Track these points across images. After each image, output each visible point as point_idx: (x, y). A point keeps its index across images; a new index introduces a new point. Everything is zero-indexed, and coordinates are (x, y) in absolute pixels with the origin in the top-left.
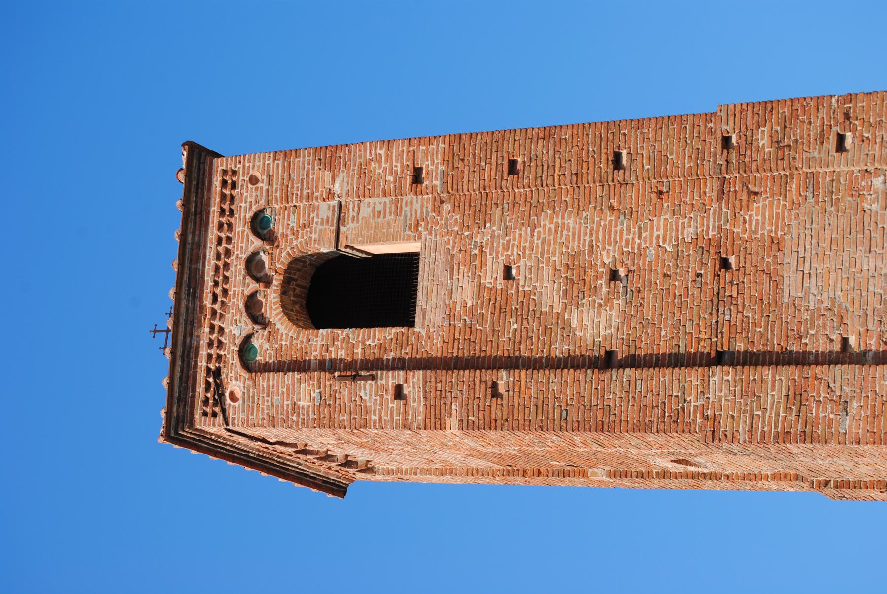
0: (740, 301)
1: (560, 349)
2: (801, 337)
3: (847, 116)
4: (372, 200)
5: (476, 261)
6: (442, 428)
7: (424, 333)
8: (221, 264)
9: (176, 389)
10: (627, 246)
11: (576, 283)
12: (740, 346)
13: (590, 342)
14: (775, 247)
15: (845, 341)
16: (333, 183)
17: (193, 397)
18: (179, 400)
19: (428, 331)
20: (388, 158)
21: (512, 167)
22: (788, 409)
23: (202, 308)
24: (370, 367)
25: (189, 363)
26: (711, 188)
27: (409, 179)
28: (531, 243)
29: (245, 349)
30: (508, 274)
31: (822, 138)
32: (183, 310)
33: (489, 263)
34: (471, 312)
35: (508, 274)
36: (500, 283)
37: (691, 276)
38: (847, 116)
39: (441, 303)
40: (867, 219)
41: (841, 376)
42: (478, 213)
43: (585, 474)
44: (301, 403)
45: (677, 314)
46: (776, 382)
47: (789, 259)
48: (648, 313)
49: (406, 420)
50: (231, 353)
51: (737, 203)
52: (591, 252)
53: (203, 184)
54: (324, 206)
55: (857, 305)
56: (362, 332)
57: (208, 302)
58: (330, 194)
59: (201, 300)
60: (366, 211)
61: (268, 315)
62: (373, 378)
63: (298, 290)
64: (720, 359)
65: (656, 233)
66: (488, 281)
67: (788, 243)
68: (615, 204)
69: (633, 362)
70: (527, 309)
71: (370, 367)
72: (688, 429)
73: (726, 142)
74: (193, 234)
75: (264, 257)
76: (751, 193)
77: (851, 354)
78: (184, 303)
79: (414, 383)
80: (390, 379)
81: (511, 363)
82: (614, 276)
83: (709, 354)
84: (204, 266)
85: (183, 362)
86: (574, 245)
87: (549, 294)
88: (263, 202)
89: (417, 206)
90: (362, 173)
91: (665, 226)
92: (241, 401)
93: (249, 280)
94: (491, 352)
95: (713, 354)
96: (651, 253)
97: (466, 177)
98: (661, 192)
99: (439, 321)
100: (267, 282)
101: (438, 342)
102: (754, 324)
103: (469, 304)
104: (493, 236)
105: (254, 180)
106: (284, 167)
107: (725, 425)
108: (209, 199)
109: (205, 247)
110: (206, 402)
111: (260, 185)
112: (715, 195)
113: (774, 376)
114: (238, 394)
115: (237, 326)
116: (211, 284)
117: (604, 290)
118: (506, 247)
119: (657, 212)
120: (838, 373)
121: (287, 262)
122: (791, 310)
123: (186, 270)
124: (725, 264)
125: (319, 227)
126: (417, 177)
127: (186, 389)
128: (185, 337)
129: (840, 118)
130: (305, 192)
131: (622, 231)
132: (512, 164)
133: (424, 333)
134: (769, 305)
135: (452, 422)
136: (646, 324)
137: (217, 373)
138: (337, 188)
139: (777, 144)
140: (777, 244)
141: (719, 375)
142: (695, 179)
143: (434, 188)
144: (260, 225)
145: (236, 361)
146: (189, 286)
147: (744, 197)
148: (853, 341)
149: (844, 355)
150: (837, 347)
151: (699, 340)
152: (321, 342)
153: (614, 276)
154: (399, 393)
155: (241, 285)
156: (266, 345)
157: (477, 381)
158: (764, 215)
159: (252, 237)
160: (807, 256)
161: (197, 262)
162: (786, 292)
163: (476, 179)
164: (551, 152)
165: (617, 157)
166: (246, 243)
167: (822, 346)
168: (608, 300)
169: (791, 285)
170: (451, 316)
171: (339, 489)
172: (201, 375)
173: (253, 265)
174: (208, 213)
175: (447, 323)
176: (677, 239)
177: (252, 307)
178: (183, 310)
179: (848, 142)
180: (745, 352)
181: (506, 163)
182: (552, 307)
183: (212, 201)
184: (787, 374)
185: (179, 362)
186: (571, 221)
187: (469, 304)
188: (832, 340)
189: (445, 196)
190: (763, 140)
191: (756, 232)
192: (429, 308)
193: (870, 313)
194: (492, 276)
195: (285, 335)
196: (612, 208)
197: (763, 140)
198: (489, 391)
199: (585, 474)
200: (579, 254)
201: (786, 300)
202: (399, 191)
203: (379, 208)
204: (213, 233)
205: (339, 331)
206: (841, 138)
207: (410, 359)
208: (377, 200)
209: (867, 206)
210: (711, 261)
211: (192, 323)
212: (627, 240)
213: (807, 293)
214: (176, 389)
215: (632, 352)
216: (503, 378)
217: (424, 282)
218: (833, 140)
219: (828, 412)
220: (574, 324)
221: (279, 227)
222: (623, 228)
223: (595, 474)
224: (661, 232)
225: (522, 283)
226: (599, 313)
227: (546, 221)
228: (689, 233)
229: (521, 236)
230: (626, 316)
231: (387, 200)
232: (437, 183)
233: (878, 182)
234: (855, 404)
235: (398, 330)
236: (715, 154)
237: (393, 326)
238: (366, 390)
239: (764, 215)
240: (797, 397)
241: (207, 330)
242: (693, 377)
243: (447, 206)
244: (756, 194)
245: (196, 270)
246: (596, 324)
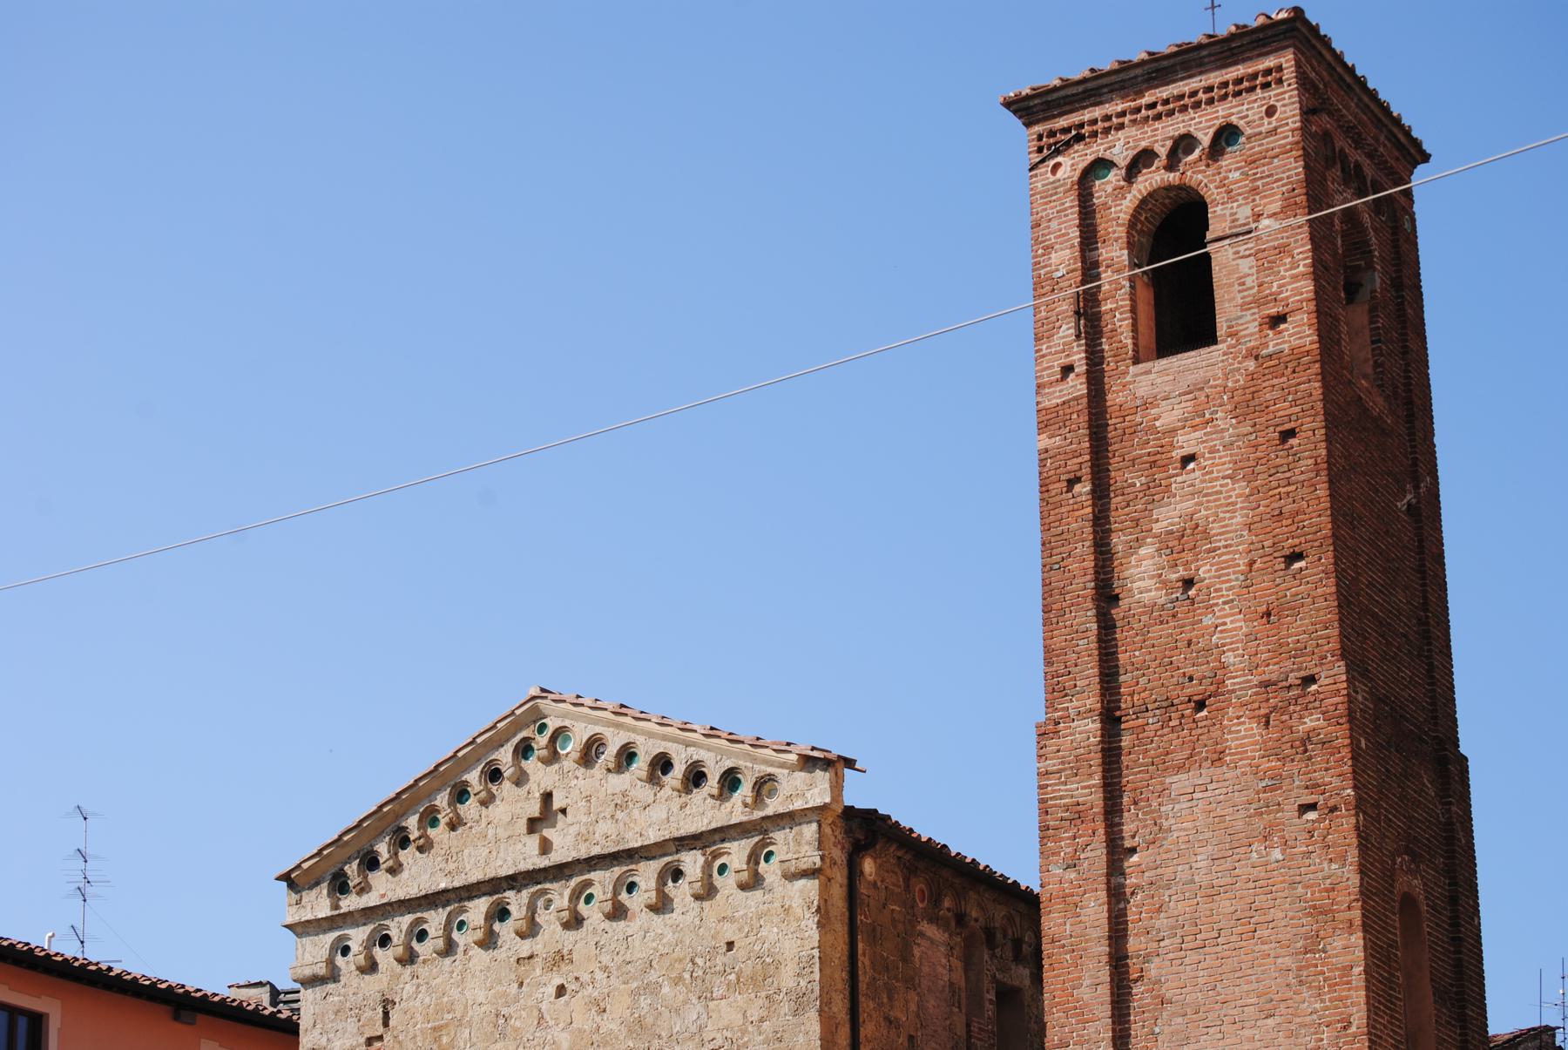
0: (1166, 730)
1: (1118, 541)
2: (1135, 803)
3: (1334, 809)
5: (1199, 419)
6: (1041, 431)
7: (1128, 379)
8: (1186, 100)
9: (1055, 96)
10: (1216, 591)
11: (1186, 541)
12: (1126, 741)
13: (1127, 574)
14: (1215, 756)
15: (1133, 851)
16: (1269, 216)
17: (1054, 117)
18: (1047, 102)
19: (1130, 383)
20: (1295, 278)
22: (1067, 808)
23: (1140, 94)
25: (1083, 99)
26: (1272, 672)
27: (1273, 311)
28: (1217, 479)
29: (1101, 165)
30: (1188, 459)
31: (1312, 787)
32: (1132, 73)
33: (1198, 434)
34: (1152, 429)
35: (1188, 459)
36: (1177, 454)
37: (1189, 670)
38: (1334, 809)
39: (1159, 388)
40: (1242, 850)
41: (1097, 854)
44: (1053, 255)
45: (1153, 665)
47: (1207, 772)
48: (1156, 630)
50: (1097, 149)
51: (1256, 705)
52: (1209, 551)
53: (1264, 46)
55: (1165, 856)
57: (1147, 98)
58: (1258, 217)
59: (1148, 89)
61: (1140, 179)
62: (1078, 337)
64: (1111, 720)
65: (1228, 620)
66: (1181, 438)
67: (1219, 770)
68: (1256, 566)
70: (1155, 492)
72: (1050, 706)
73: (1310, 680)
74: (1210, 55)
75: (1197, 153)
76: (1267, 717)
77: (1122, 861)
78: (1139, 71)
79: (1077, 386)
80: (1078, 358)
82: (1188, 583)
83: (1119, 708)
84: (1182, 79)
85: (1084, 92)
86: (1215, 528)
87: (1167, 517)
88: (1248, 131)
91: (1235, 629)
92: (1052, 179)
93: (1169, 143)
94: (1115, 463)
95: (1118, 713)
96: (1208, 620)
97: (1275, 381)
98: (1269, 615)
99: (1140, 393)
100: (1171, 166)
102: (1146, 751)
103: (1157, 423)
104: (1223, 431)
105: (1271, 111)
106: (1284, 146)
107: (1052, 744)
108: (1250, 59)
109: (1201, 73)
111: (1266, 121)
112: (1266, 677)
114: (1060, 174)
115: (1119, 148)
116: (1164, 95)
117: (1174, 576)
118: (1213, 451)
120: (1098, 852)
121: (1193, 184)
122: (1159, 788)
123: (1172, 61)
124: (1201, 705)
125: (1228, 212)
127: (1059, 106)
129: (1331, 803)
130: (1259, 183)
131: (1228, 581)
132: (1291, 433)
133: (1128, 379)
134: (1162, 764)
135: (1044, 441)
136: (1145, 631)
137: (1079, 138)
138: (1265, 222)
139: (1306, 739)
140: (1218, 758)
141: (1093, 726)
142: (1279, 650)
143: (1266, 345)
144: (1227, 135)
145: (1090, 158)
146: (1157, 71)
147: (1263, 711)
148: (1135, 859)
149: (1117, 853)
150: (1128, 844)
151: (1132, 695)
153: (1188, 583)
154: (1067, 370)
155: (1160, 136)
156: (1109, 189)
157: (1080, 460)
158: (1245, 737)
159: (1211, 131)
160: (1208, 794)
161: (1186, 69)
162: (1175, 778)
163: (1276, 394)
164: (1302, 477)
165: (1298, 556)
166: (1202, 125)
167: (1128, 828)
168: (1164, 583)
169: (1179, 782)
170: (1146, 405)
172: (1075, 118)
173: (1184, 143)
174: (1235, 63)
175: (1138, 402)
176: (1224, 645)
177: (1143, 159)
178: (1132, 73)
179: (1312, 815)
180: (1120, 748)
181: (1292, 425)
182: (1157, 521)
183: (1249, 63)
184: (1096, 799)
185: (1080, 88)
186: (1239, 519)
187: (1157, 423)
188: (1133, 837)
190: (1311, 722)
191: (1230, 732)
192: (1153, 376)
194: (1187, 442)
195: (1118, 204)
196: (1251, 563)
197: (1311, 722)
198: (1072, 476)
200: (1207, 536)
201: (1168, 780)
204: (1215, 78)
206: (1312, 807)
207: (1103, 371)
209: (1254, 847)
211: (1123, 88)
212: (1220, 590)
213: (1175, 801)
214: (1055, 96)
215: (1118, 624)
216: (1083, 488)
218: (1310, 799)
219: (1067, 849)
220: (1142, 551)
221: (1230, 160)
224: (1229, 626)
225: (1179, 479)
226: (1152, 577)
227: (1241, 488)
228: (1229, 658)
229: (1222, 463)
233: (1277, 854)
234: (1073, 876)
236: (1299, 669)
238: (1067, 331)
239: (1245, 737)
241: (1119, 108)
242: (1092, 701)
243: (1251, 365)
244: (1267, 723)
245: (1176, 72)
246: (1143, 576)
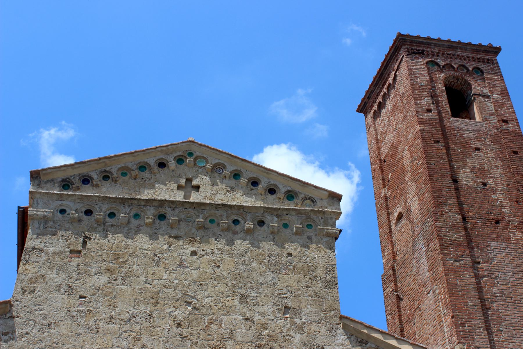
4: (492, 106)
5: (479, 139)
21: (515, 153)
24: (436, 103)
28: (490, 157)
42: (496, 140)
43: (384, 186)
46: (459, 236)
47: (504, 245)
49: (420, 112)
54: (487, 91)
56: (446, 100)
58: (492, 93)
60: (489, 104)
63: (453, 83)
69: (456, 189)
71: (436, 103)
79: (433, 115)
81: (447, 148)
87: (472, 162)
89: (494, 121)
90: (502, 104)
96: (494, 197)
101: (448, 125)
104: (489, 145)
110: (412, 49)
113: (462, 236)
119: (510, 200)
124: (497, 222)
126: (506, 121)
128: (434, 44)
152: (441, 87)
171: (363, 108)
189: (500, 130)
193: (491, 272)
194: (474, 144)
199: (384, 186)
202: (498, 115)
203: (491, 109)
205: (445, 93)
208: (493, 108)
210: (496, 218)
216: (442, 144)
217: (468, 121)
222: (502, 187)
223: (385, 190)
228: (505, 210)
230: (470, 187)
231: (494, 111)
232: (504, 127)
235: (450, 112)
237: (451, 110)
238: (427, 100)
240: (456, 244)
243: (496, 131)
246: (466, 177)
